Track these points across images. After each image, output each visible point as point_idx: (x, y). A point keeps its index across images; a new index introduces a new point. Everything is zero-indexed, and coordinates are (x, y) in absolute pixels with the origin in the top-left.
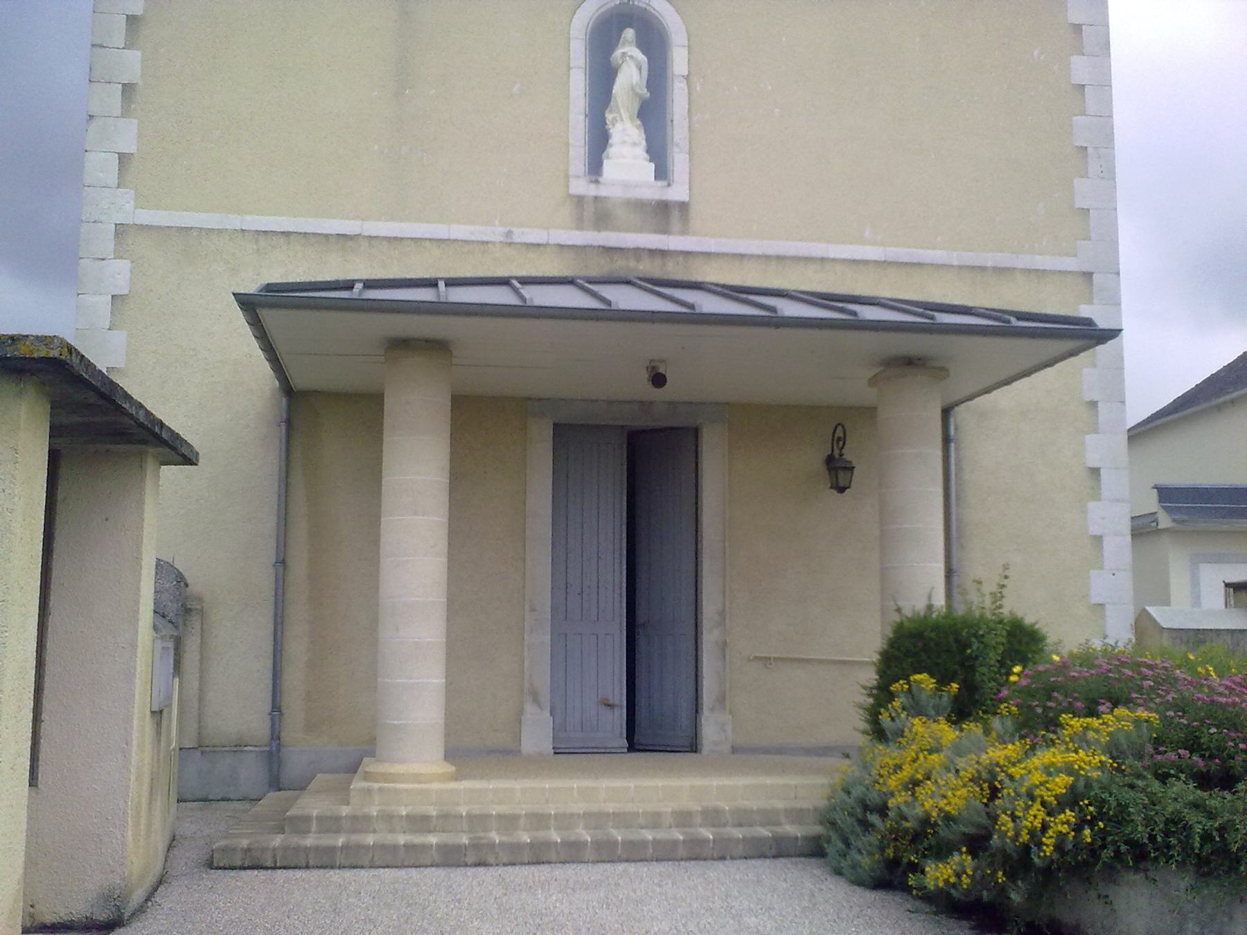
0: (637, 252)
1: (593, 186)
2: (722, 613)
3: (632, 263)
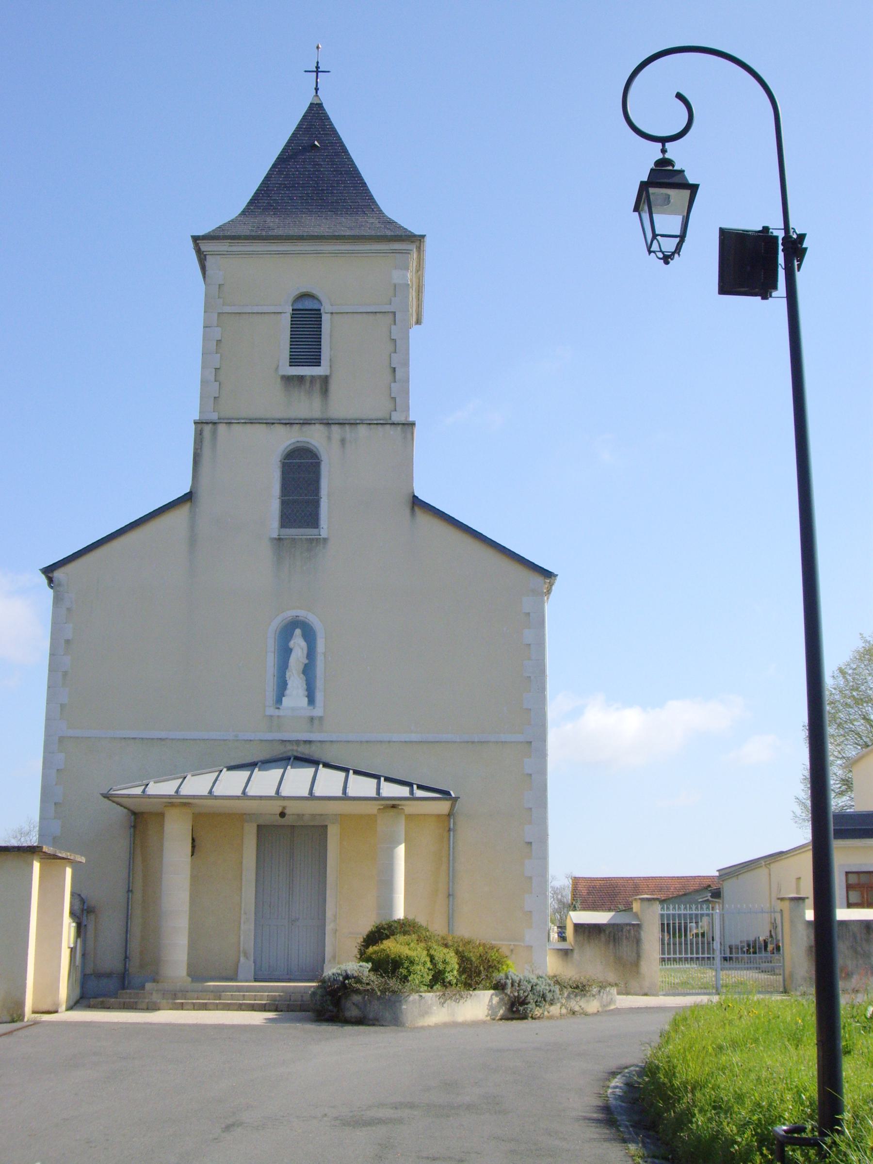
2: (335, 916)
3: (295, 748)
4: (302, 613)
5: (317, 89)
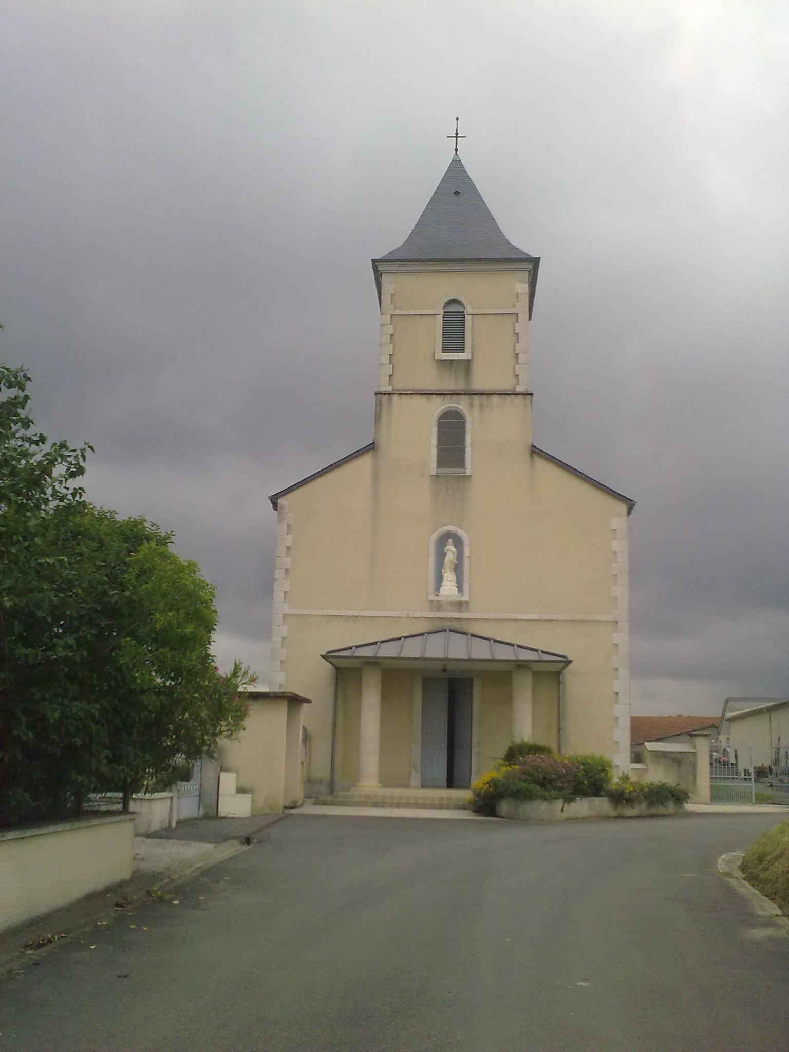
0: (451, 619)
1: (436, 597)
4: (453, 528)
5: (456, 150)
